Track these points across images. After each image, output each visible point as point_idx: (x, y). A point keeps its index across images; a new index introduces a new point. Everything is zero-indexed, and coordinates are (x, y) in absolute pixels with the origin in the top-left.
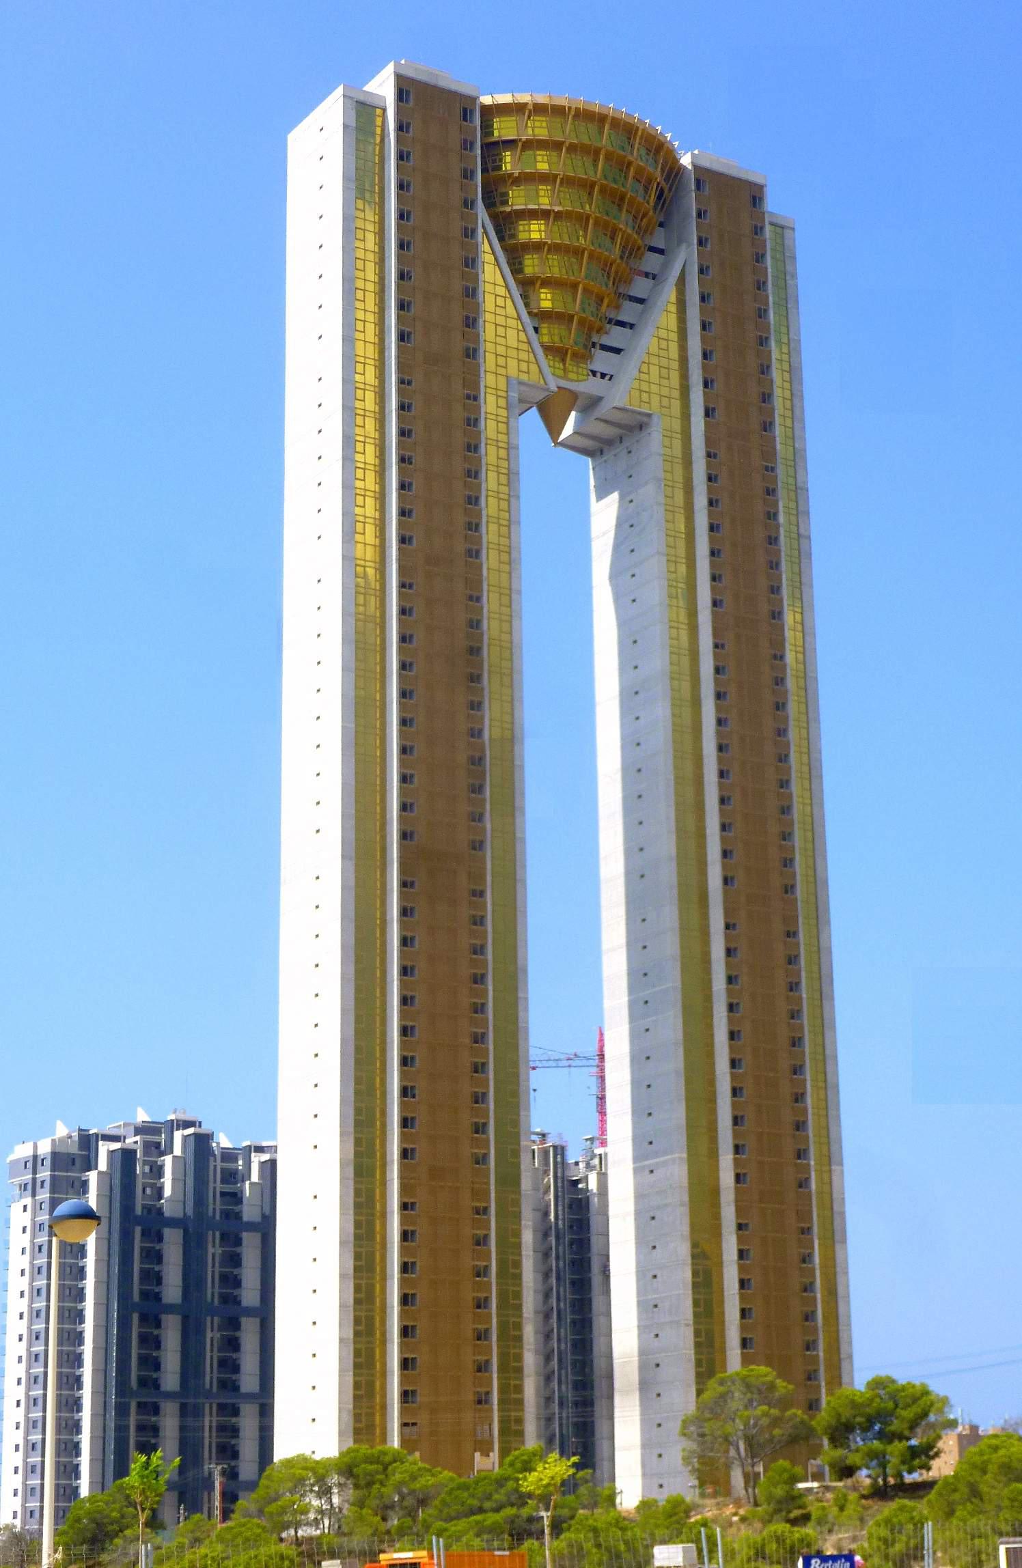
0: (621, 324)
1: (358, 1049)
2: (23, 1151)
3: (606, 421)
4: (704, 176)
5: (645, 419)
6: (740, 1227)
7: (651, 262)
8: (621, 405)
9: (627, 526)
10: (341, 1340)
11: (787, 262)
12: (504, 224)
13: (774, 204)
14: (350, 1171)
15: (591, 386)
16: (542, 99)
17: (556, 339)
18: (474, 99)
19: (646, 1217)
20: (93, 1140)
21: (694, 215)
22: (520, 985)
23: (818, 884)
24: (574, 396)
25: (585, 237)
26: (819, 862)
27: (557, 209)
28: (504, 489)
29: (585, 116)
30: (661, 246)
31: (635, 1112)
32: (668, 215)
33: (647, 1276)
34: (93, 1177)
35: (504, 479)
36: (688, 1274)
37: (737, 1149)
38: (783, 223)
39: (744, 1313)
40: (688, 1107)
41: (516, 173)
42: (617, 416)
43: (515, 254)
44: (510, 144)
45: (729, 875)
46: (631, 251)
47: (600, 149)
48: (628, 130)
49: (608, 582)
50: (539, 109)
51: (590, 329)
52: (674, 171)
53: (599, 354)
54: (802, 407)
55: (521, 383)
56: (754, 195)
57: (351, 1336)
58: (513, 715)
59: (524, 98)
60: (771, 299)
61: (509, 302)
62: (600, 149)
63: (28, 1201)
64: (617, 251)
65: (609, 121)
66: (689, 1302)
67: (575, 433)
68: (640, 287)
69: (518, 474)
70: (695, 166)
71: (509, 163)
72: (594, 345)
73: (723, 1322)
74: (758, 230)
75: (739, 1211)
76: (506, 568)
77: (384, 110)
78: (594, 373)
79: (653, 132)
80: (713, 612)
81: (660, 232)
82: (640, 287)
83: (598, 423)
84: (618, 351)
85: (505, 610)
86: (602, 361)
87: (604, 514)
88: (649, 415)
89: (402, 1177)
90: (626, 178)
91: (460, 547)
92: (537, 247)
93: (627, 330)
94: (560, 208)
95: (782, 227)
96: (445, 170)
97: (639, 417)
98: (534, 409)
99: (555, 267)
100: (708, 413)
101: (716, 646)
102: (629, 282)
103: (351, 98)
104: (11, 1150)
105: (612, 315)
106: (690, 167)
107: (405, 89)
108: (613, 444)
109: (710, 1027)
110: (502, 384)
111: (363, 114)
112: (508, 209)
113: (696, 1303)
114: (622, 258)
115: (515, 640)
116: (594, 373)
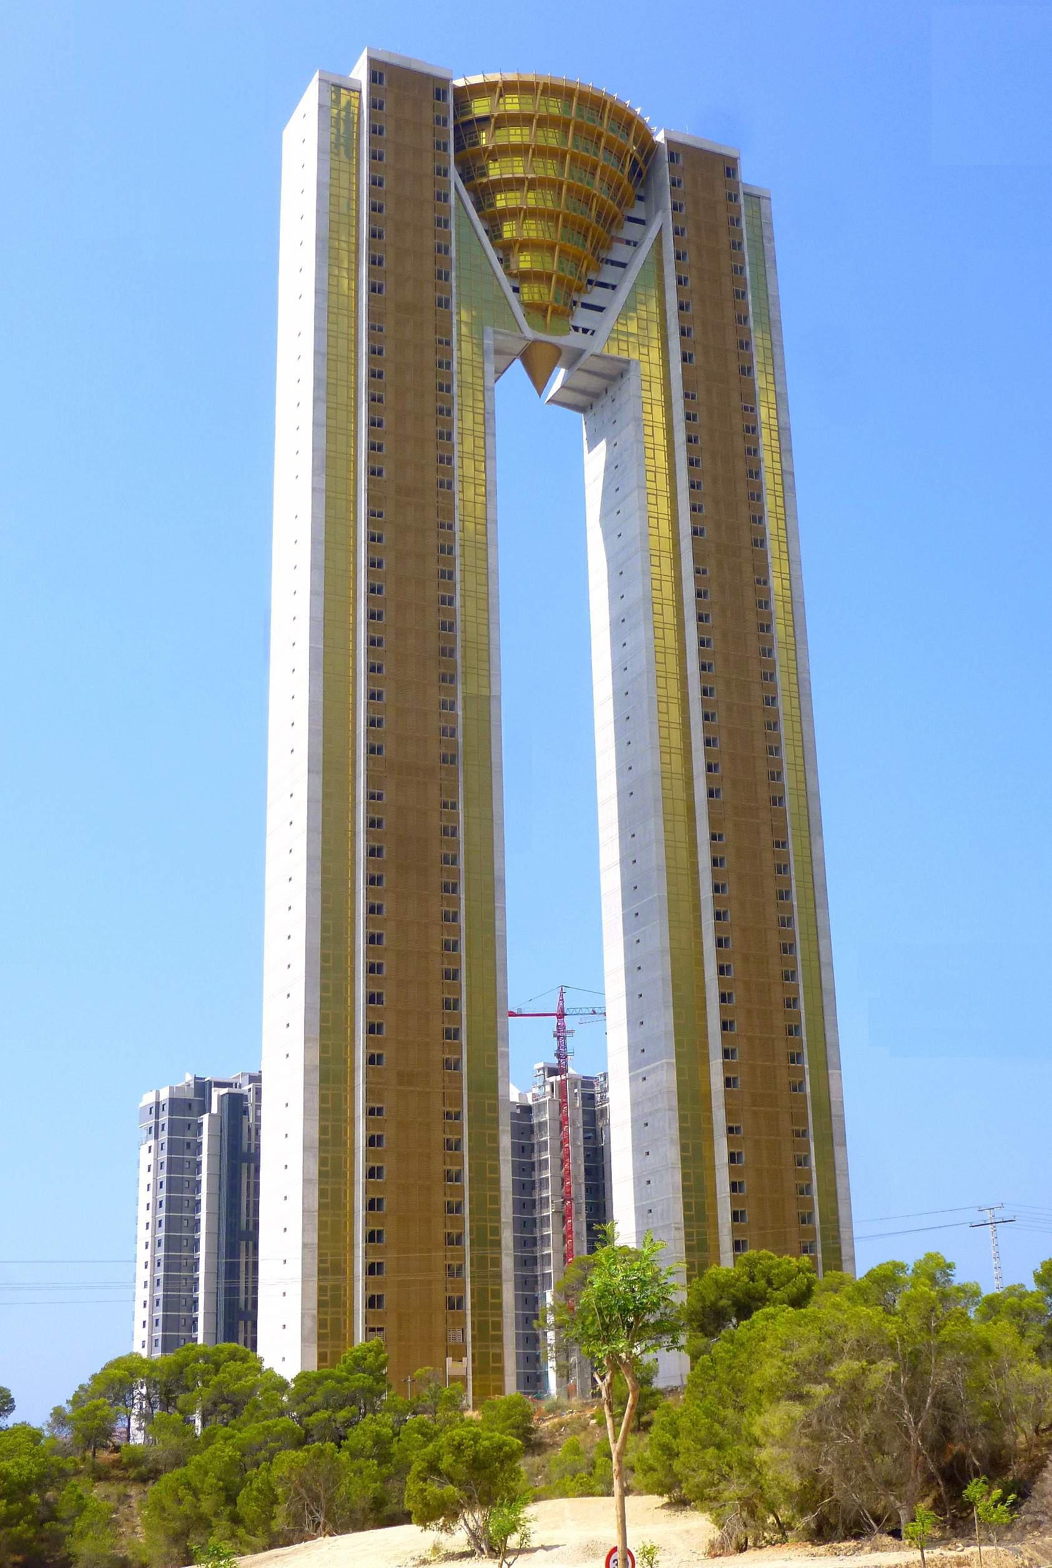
1: (325, 958)
2: (149, 1099)
3: (589, 372)
4: (676, 150)
6: (730, 1130)
7: (631, 231)
8: (598, 351)
10: (305, 1246)
13: (749, 175)
15: (573, 340)
16: (511, 77)
17: (536, 297)
18: (447, 81)
19: (641, 1124)
20: (207, 1087)
21: (668, 183)
22: (497, 894)
23: (809, 797)
26: (809, 776)
31: (629, 1022)
32: (645, 185)
33: (643, 1182)
34: (205, 1119)
35: (479, 419)
37: (726, 1054)
38: (756, 193)
39: (736, 1216)
40: (676, 1016)
42: (598, 365)
44: (484, 120)
47: (570, 120)
48: (594, 103)
50: (508, 88)
52: (649, 149)
53: (579, 311)
56: (729, 167)
57: (316, 1241)
59: (494, 77)
62: (570, 120)
63: (152, 1143)
65: (577, 94)
66: (679, 1206)
67: (562, 387)
68: (620, 252)
73: (716, 1225)
74: (733, 197)
75: (729, 1114)
76: (481, 499)
77: (360, 92)
78: (576, 329)
81: (638, 202)
82: (620, 252)
83: (581, 374)
84: (601, 309)
86: (583, 318)
87: (595, 462)
88: (628, 362)
89: (367, 1083)
90: (598, 148)
92: (512, 214)
93: (609, 291)
94: (533, 176)
96: (419, 144)
97: (617, 363)
98: (518, 363)
99: (532, 230)
103: (327, 82)
104: (141, 1101)
107: (378, 73)
108: (598, 394)
109: (698, 935)
111: (335, 89)
112: (484, 180)
113: (687, 1206)
114: (597, 222)
116: (576, 329)
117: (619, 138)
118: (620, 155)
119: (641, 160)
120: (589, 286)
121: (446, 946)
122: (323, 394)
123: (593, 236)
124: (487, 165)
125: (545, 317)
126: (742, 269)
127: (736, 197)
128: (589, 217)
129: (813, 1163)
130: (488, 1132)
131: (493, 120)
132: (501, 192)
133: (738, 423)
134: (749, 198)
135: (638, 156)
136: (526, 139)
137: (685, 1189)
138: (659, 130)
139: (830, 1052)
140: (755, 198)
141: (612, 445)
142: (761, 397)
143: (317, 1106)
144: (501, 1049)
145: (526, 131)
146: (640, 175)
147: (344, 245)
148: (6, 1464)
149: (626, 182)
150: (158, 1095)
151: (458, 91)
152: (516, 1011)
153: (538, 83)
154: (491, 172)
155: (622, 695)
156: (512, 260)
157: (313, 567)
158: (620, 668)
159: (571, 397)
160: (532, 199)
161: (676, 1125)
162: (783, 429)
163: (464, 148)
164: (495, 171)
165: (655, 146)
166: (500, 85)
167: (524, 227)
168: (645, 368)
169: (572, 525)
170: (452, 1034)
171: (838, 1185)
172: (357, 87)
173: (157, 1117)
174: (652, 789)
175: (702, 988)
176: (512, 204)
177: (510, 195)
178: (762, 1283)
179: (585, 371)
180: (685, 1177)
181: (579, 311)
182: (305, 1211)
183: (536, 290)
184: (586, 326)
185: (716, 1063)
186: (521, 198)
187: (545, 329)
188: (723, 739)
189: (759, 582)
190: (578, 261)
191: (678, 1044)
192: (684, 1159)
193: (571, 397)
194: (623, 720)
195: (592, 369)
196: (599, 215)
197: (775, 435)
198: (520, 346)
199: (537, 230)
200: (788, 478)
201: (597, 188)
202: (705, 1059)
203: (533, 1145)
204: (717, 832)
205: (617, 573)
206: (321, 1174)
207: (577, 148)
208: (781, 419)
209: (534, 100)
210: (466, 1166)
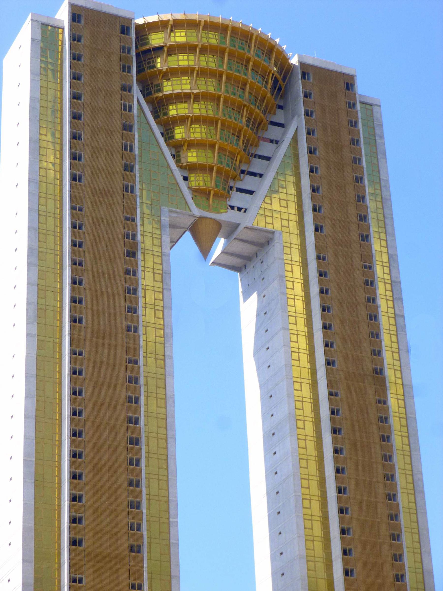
0: (254, 174)
4: (306, 70)
5: (270, 235)
7: (273, 132)
8: (249, 225)
9: (263, 314)
11: (376, 128)
13: (363, 89)
16: (179, 16)
18: (130, 20)
21: (301, 95)
24: (218, 225)
27: (195, 91)
28: (160, 285)
30: (282, 122)
35: (158, 278)
41: (164, 69)
42: (250, 235)
44: (159, 49)
45: (349, 568)
46: (258, 125)
47: (225, 49)
48: (244, 36)
49: (253, 358)
50: (177, 25)
51: (227, 176)
52: (286, 70)
53: (234, 193)
54: (393, 225)
56: (348, 83)
58: (167, 448)
60: (363, 151)
62: (225, 49)
64: (244, 120)
65: (230, 29)
67: (223, 252)
68: (265, 149)
71: (159, 63)
72: (231, 188)
74: (352, 105)
77: (63, 29)
78: (232, 208)
79: (265, 37)
80: (327, 369)
81: (279, 111)
83: (237, 242)
84: (251, 192)
85: (161, 371)
86: (237, 199)
87: (249, 309)
88: (273, 233)
90: (247, 69)
91: (122, 323)
92: (182, 120)
95: (371, 105)
98: (188, 235)
99: (198, 132)
100: (317, 229)
101: (331, 394)
103: (38, 21)
105: (244, 167)
106: (297, 64)
108: (251, 256)
111: (46, 34)
112: (160, 95)
114: (248, 126)
115: (169, 393)
116: (232, 208)
119: (280, 78)
120: (242, 175)
122: (35, 260)
123: (244, 136)
124: (162, 83)
125: (208, 199)
126: (360, 160)
127: (354, 105)
131: (166, 49)
132: (173, 103)
135: (278, 76)
136: (192, 63)
138: (293, 56)
140: (369, 106)
141: (262, 296)
142: (377, 257)
145: (192, 57)
146: (280, 89)
149: (269, 95)
153: (200, 21)
154: (165, 89)
156: (182, 155)
158: (272, 472)
160: (197, 109)
162: (395, 282)
163: (143, 70)
164: (168, 88)
166: (171, 22)
168: (285, 237)
176: (182, 112)
177: (180, 106)
181: (234, 193)
183: (201, 178)
190: (233, 156)
194: (275, 514)
196: (248, 121)
198: (189, 222)
200: (400, 320)
208: (393, 275)
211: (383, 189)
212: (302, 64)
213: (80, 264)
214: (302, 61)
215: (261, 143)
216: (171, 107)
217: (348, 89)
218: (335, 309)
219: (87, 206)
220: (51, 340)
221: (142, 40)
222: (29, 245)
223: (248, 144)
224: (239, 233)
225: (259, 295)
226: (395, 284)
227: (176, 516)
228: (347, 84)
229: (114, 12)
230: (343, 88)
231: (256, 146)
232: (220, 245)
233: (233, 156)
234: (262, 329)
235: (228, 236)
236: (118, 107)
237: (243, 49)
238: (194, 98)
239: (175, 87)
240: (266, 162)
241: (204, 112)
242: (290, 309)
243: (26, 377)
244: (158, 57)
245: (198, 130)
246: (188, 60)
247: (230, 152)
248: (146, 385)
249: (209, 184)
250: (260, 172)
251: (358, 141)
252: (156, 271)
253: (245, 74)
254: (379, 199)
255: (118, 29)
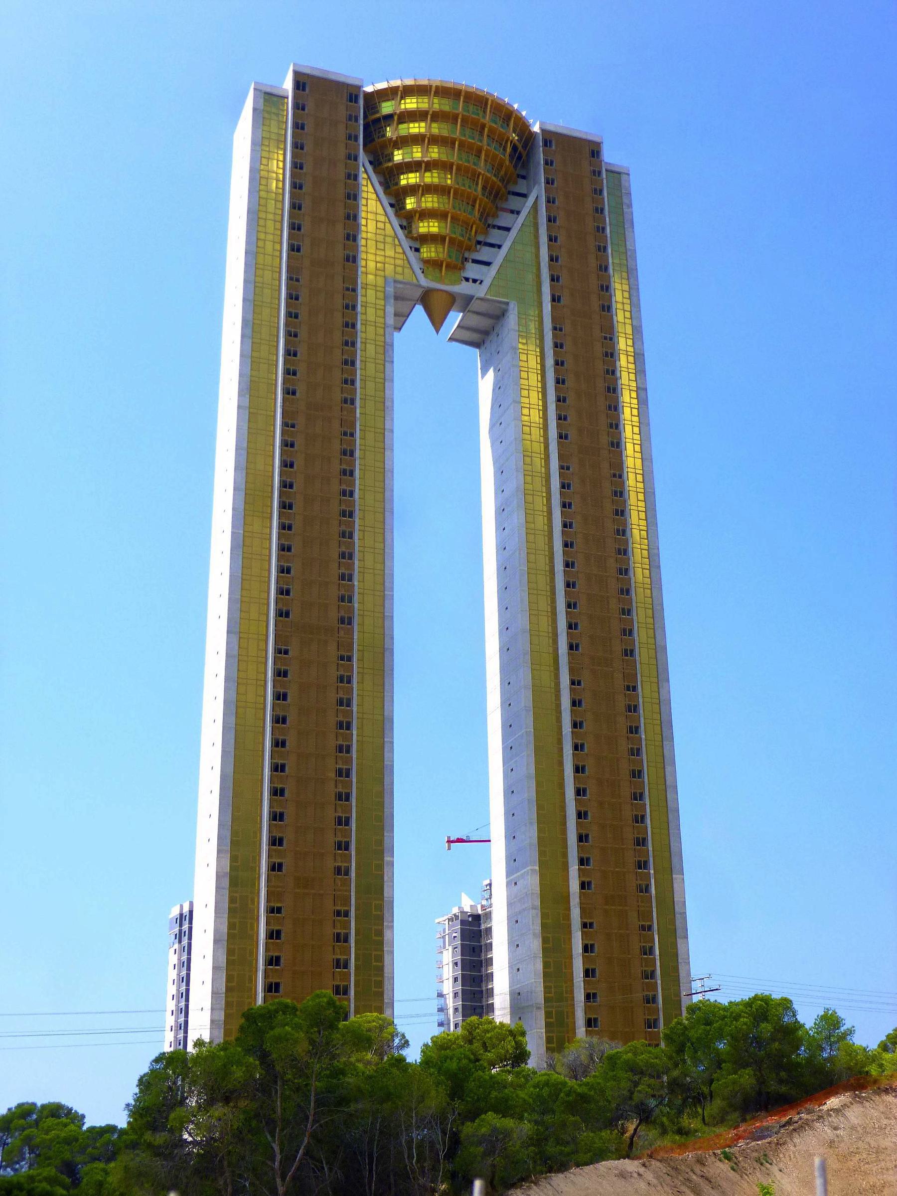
0: (492, 245)
4: (550, 138)
5: (504, 306)
6: (584, 925)
12: (389, 177)
13: (610, 156)
14: (226, 882)
16: (409, 82)
18: (359, 88)
19: (514, 921)
21: (542, 162)
23: (659, 651)
25: (451, 179)
27: (426, 159)
29: (443, 92)
36: (540, 966)
37: (582, 862)
40: (540, 830)
43: (396, 196)
44: (389, 117)
47: (458, 115)
48: (477, 100)
50: (408, 91)
53: (469, 265)
55: (395, 281)
56: (594, 150)
61: (388, 226)
62: (458, 115)
63: (176, 946)
65: (463, 93)
69: (392, 345)
70: (543, 130)
77: (287, 98)
78: (467, 280)
81: (520, 181)
86: (472, 270)
87: (486, 384)
92: (412, 190)
93: (496, 249)
95: (619, 173)
96: (333, 132)
98: (419, 310)
99: (430, 202)
102: (390, 157)
107: (301, 82)
110: (380, 281)
111: (269, 100)
112: (390, 164)
114: (483, 195)
116: (467, 280)
117: (498, 127)
118: (502, 141)
119: (520, 146)
120: (478, 246)
121: (340, 773)
122: (249, 332)
123: (480, 206)
125: (441, 270)
126: (604, 229)
127: (600, 173)
128: (476, 190)
129: (657, 952)
130: (374, 927)
131: (396, 118)
132: (403, 173)
133: (598, 350)
134: (611, 174)
135: (517, 143)
136: (423, 130)
137: (546, 975)
138: (535, 123)
139: (675, 860)
140: (617, 175)
141: (497, 370)
142: (620, 328)
143: (227, 906)
144: (387, 859)
145: (423, 124)
146: (520, 157)
147: (271, 216)
148: (281, 1190)
149: (507, 163)
150: (182, 906)
151: (368, 96)
152: (465, 838)
153: (431, 86)
155: (503, 569)
156: (414, 226)
157: (236, 468)
158: (502, 548)
159: (468, 335)
160: (431, 178)
161: (539, 921)
162: (638, 354)
163: (373, 140)
164: (398, 156)
165: (532, 136)
166: (401, 89)
167: (432, 206)
169: (455, 432)
170: (344, 846)
171: (681, 971)
172: (285, 95)
173: (181, 925)
174: (523, 643)
175: (563, 808)
177: (411, 175)
178: (477, 1045)
179: (475, 312)
180: (546, 965)
181: (469, 265)
182: (214, 993)
183: (433, 249)
184: (476, 277)
185: (574, 868)
186: (420, 177)
187: (441, 280)
188: (582, 603)
189: (614, 476)
190: (467, 225)
191: (542, 853)
192: (545, 950)
193: (468, 335)
194: (503, 589)
195: (480, 311)
196: (484, 188)
197: (631, 359)
198: (418, 293)
199: (433, 201)
200: (642, 393)
201: (482, 167)
202: (566, 867)
203: (481, 946)
204: (576, 679)
205: (500, 471)
206: (228, 962)
207: (465, 136)
208: (636, 347)
209: (429, 99)
210: (353, 956)
211: (629, 260)
212: (543, 131)
213: (296, 336)
214: (543, 127)
215: (500, 213)
216: (402, 177)
217: (593, 156)
218: (570, 382)
219: (305, 277)
220: (264, 412)
221: (372, 108)
222: (243, 317)
223: (485, 215)
224: (475, 305)
225: (494, 371)
226: (639, 358)
227: (392, 589)
228: (593, 152)
229: (342, 79)
230: (588, 155)
231: (493, 216)
232: (455, 319)
233: (467, 225)
234: (497, 404)
235: (463, 310)
236: (342, 176)
237: (478, 114)
238: (426, 167)
239: (406, 156)
240: (506, 233)
241: (436, 180)
242: (523, 382)
243: (236, 449)
244: (389, 125)
245: (430, 199)
246: (419, 127)
247: (463, 222)
248: (363, 458)
249: (441, 256)
250: (498, 243)
251: (602, 210)
252: (378, 343)
253: (481, 141)
254: (625, 269)
255: (345, 96)
